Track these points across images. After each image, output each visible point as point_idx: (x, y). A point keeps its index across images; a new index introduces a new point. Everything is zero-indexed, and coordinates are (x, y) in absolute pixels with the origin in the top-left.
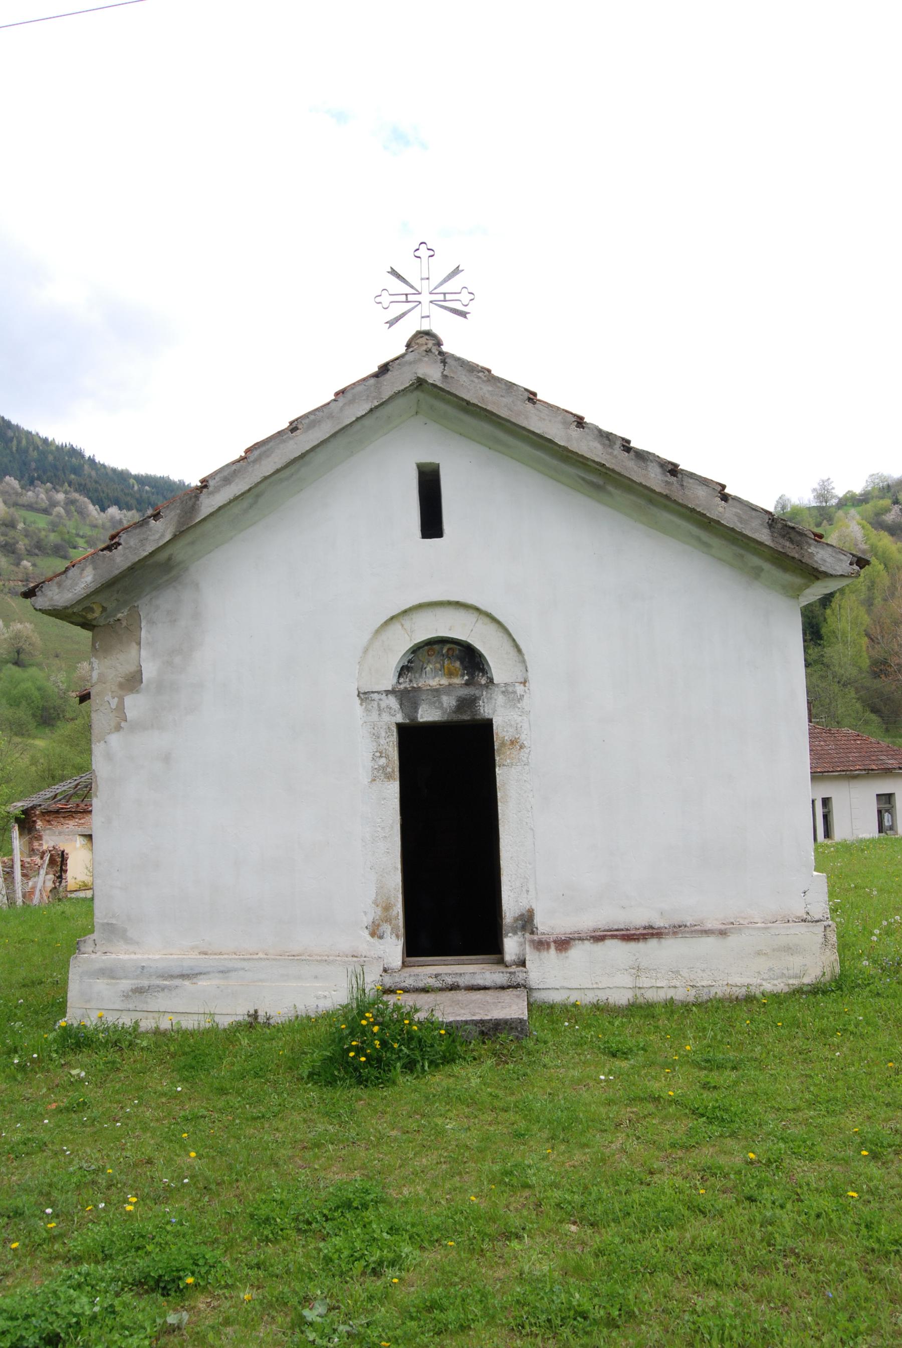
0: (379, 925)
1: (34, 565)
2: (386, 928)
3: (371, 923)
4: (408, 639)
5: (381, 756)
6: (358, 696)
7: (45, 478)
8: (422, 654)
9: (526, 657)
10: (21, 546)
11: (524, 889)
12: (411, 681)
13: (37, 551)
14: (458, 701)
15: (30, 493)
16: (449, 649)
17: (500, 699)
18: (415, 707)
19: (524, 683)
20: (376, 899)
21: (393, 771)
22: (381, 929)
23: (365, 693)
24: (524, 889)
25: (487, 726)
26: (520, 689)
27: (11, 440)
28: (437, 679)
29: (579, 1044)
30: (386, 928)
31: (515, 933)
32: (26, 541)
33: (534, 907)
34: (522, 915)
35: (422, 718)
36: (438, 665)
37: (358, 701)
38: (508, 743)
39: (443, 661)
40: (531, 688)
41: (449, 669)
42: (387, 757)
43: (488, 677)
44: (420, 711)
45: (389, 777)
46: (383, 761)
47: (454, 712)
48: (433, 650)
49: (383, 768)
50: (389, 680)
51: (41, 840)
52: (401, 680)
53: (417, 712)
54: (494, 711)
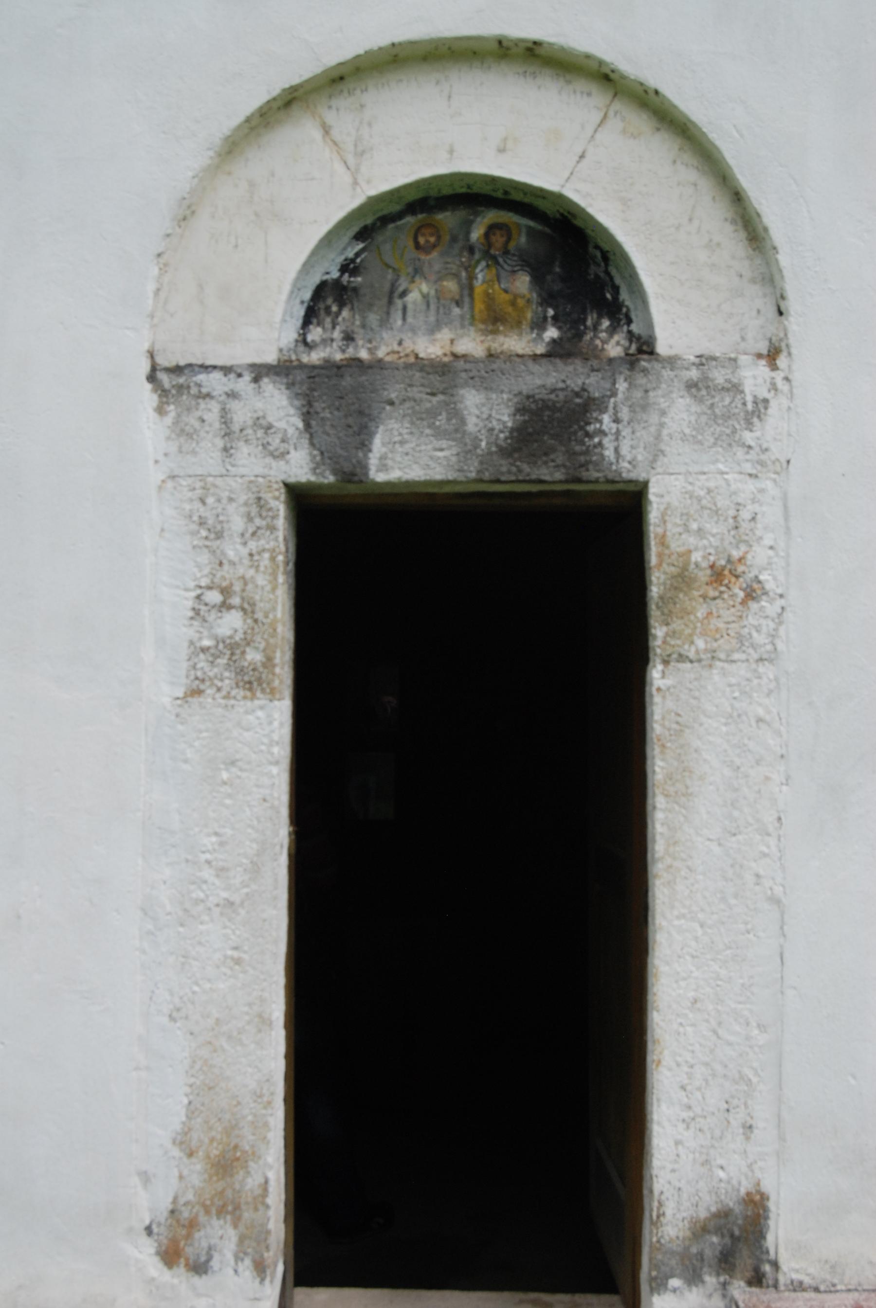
0: (192, 1225)
2: (220, 1236)
3: (163, 1215)
4: (347, 179)
5: (225, 606)
6: (152, 378)
8: (395, 244)
9: (783, 259)
11: (737, 1118)
12: (349, 338)
14: (520, 410)
16: (492, 228)
17: (678, 411)
18: (362, 435)
19: (772, 355)
20: (187, 1131)
21: (269, 662)
22: (202, 1239)
23: (177, 370)
24: (737, 1118)
25: (621, 515)
26: (754, 378)
28: (445, 335)
29: (407, 355)
30: (220, 1236)
31: (694, 1278)
33: (768, 1186)
34: (724, 1214)
35: (383, 467)
36: (451, 285)
37: (148, 396)
38: (704, 576)
39: (470, 269)
40: (796, 377)
41: (489, 299)
42: (248, 609)
43: (631, 335)
44: (378, 445)
45: (252, 683)
46: (231, 623)
47: (506, 452)
48: (436, 230)
49: (232, 648)
50: (271, 331)
51: (731, 223)
52: (315, 334)
53: (365, 446)
54: (657, 453)
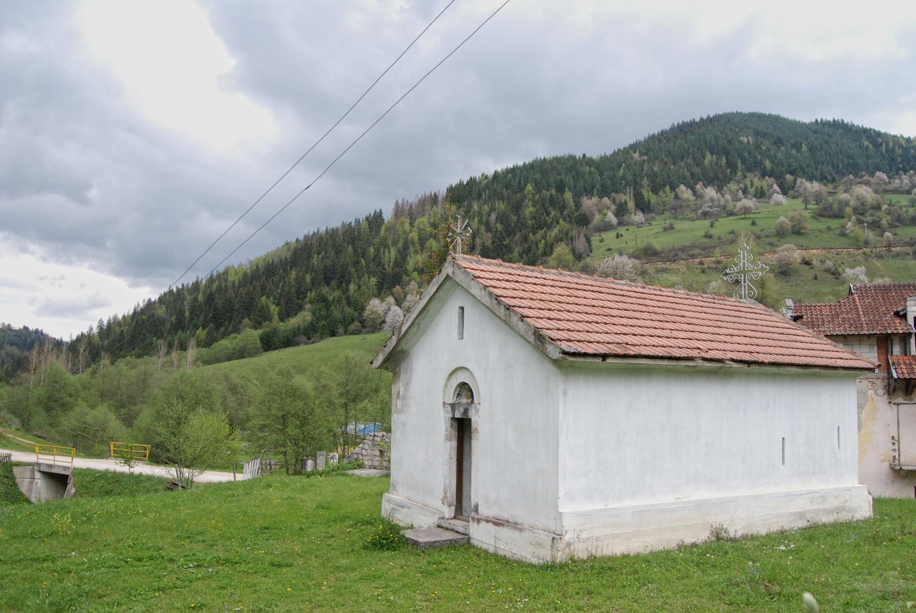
1: (895, 234)
7: (908, 167)
10: (884, 222)
13: (897, 224)
15: (897, 181)
27: (881, 144)
32: (889, 218)
